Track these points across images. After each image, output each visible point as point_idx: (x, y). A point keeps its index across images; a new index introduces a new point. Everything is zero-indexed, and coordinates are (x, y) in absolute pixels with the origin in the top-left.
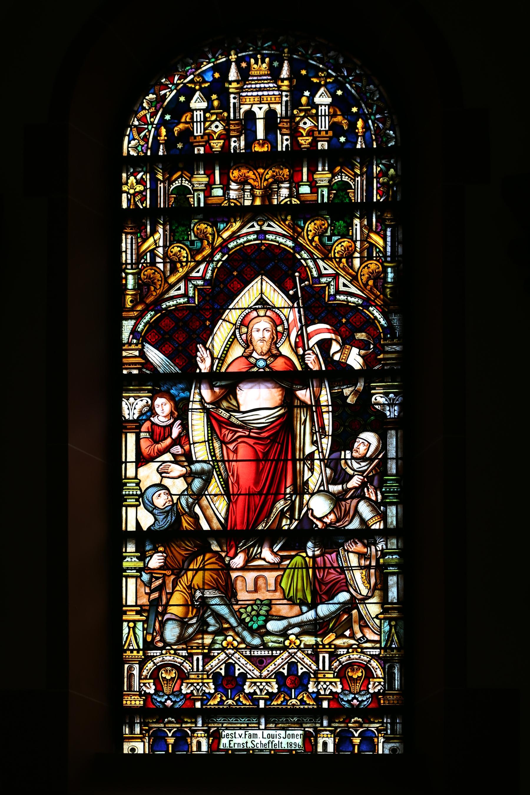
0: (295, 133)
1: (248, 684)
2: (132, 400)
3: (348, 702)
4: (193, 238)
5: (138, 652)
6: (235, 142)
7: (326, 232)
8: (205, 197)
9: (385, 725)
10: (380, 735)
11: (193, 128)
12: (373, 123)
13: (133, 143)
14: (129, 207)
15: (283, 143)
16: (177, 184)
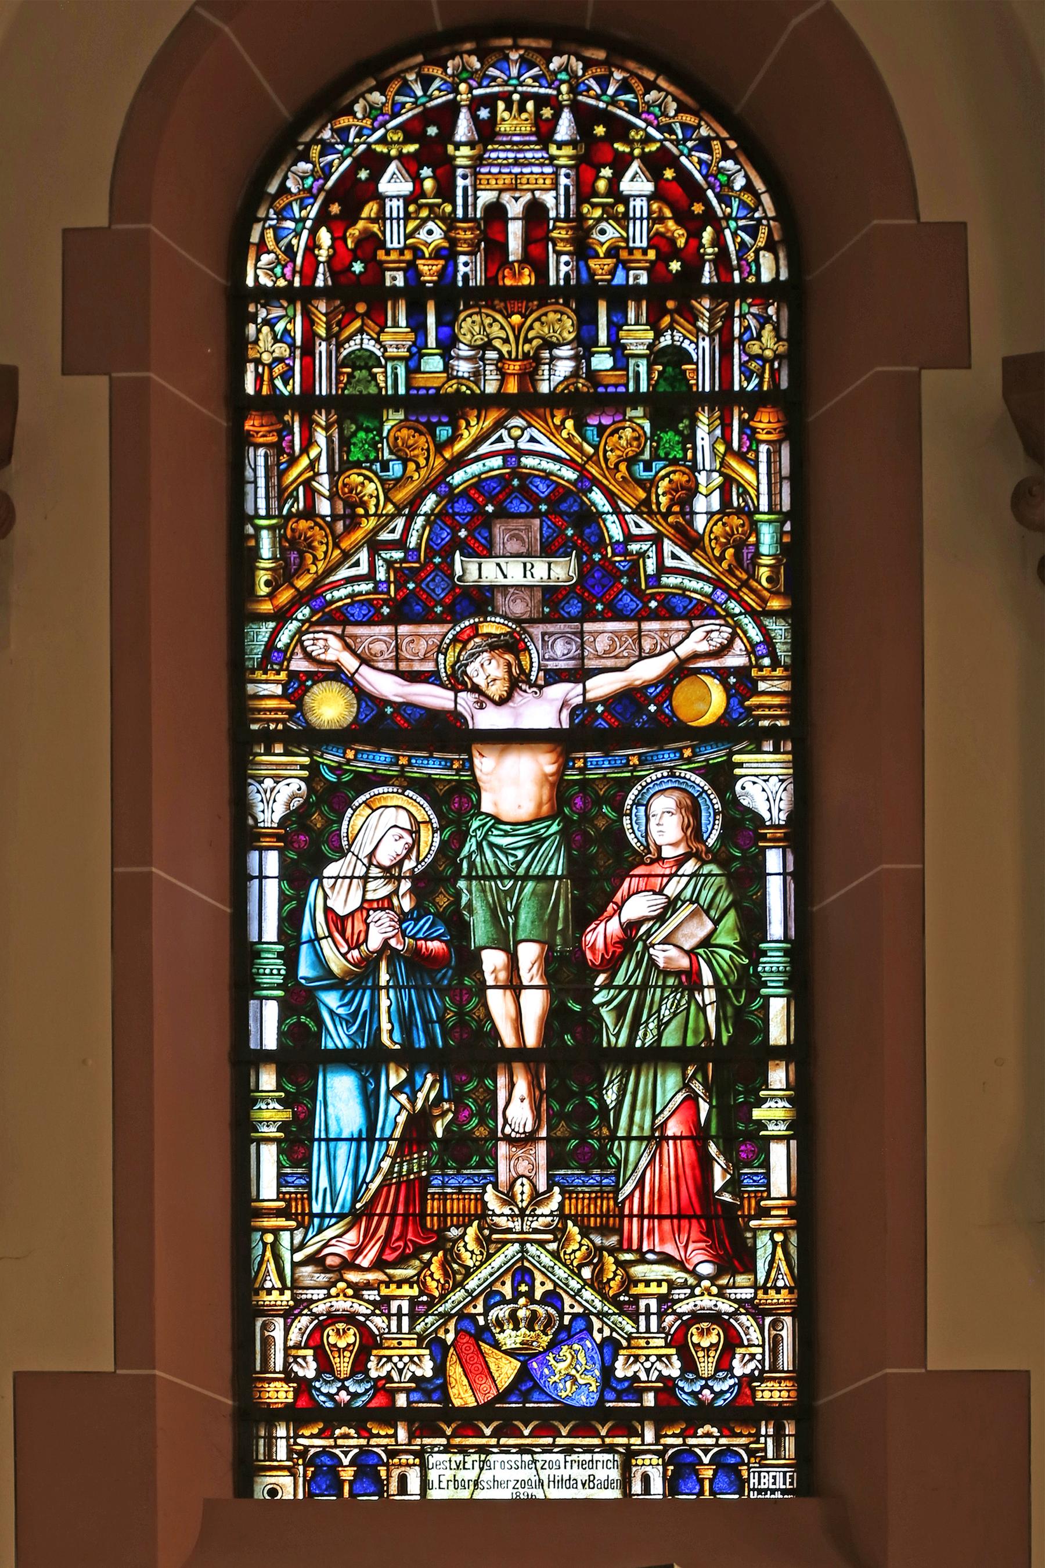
0: (583, 250)
1: (621, 1359)
2: (269, 783)
3: (694, 1394)
4: (387, 455)
5: (282, 1293)
6: (466, 264)
7: (642, 452)
8: (409, 372)
9: (762, 1440)
10: (752, 1460)
11: (384, 233)
12: (734, 235)
13: (265, 258)
14: (258, 391)
15: (560, 269)
16: (352, 346)
